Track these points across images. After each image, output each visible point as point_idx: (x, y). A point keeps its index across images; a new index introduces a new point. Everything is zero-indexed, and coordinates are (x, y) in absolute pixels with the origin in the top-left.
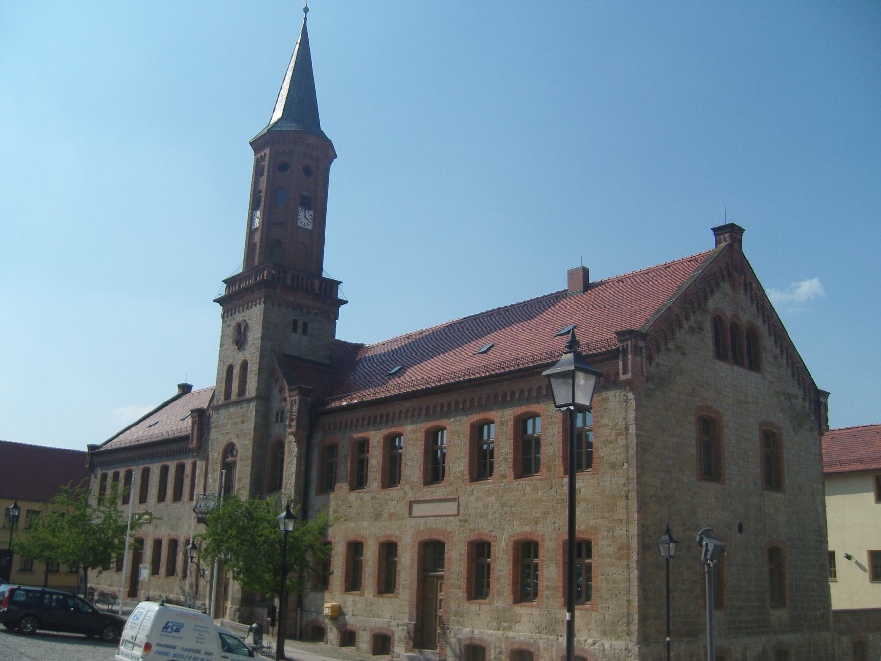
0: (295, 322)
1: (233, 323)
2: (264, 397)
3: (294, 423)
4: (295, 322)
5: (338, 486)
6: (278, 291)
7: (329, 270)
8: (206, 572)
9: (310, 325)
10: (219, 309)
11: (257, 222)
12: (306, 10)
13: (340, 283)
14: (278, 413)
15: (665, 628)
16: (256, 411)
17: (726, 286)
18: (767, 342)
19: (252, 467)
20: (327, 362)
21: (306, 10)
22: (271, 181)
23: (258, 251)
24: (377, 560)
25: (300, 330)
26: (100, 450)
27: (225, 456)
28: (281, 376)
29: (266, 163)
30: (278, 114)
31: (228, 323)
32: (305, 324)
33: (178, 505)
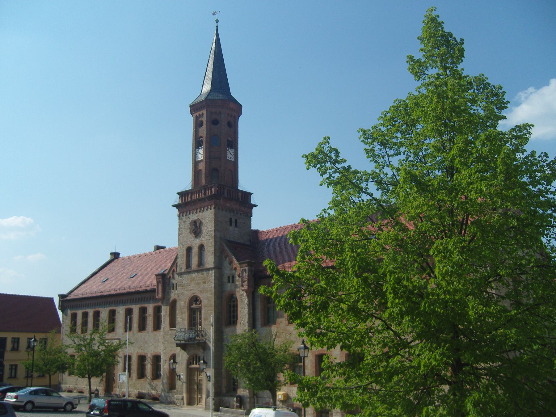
0: (231, 219)
1: (189, 221)
2: (218, 267)
3: (246, 283)
4: (231, 219)
5: (279, 320)
6: (221, 201)
7: (243, 185)
8: (182, 377)
10: (176, 211)
11: (200, 157)
12: (217, 21)
13: (252, 194)
14: (229, 278)
16: (215, 276)
19: (215, 311)
20: (248, 243)
21: (217, 21)
22: (208, 130)
23: (203, 175)
24: (314, 365)
25: (233, 224)
26: (68, 298)
27: (190, 303)
28: (230, 254)
29: (204, 119)
30: (207, 88)
31: (184, 219)
32: (236, 220)
33: (143, 334)
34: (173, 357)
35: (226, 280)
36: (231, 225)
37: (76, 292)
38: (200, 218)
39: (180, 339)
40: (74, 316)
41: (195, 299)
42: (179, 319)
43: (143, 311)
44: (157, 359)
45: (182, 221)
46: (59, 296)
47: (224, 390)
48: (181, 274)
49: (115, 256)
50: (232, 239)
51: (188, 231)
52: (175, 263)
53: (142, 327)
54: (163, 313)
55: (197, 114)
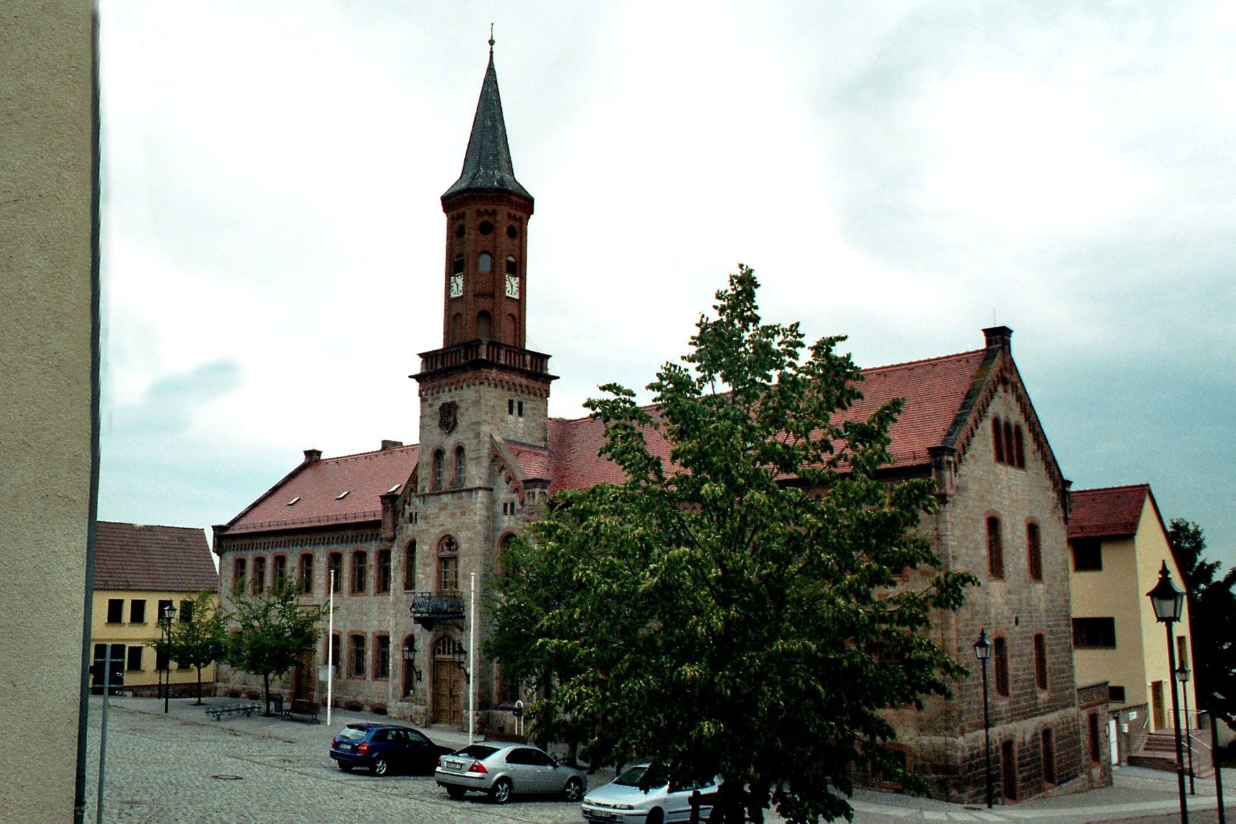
4: (511, 402)
7: (533, 343)
9: (524, 406)
10: (415, 385)
12: (492, 42)
13: (548, 357)
14: (505, 505)
15: (1177, 789)
17: (1000, 388)
18: (1028, 439)
21: (492, 42)
25: (515, 411)
26: (230, 532)
32: (520, 404)
34: (410, 642)
35: (500, 509)
36: (511, 412)
37: (243, 522)
38: (457, 399)
39: (423, 609)
40: (241, 564)
41: (449, 542)
42: (419, 575)
43: (360, 557)
44: (383, 640)
45: (427, 404)
46: (215, 528)
47: (495, 699)
48: (424, 496)
49: (313, 456)
50: (512, 438)
51: (437, 422)
52: (414, 479)
53: (359, 586)
54: (393, 564)
55: (455, 213)
